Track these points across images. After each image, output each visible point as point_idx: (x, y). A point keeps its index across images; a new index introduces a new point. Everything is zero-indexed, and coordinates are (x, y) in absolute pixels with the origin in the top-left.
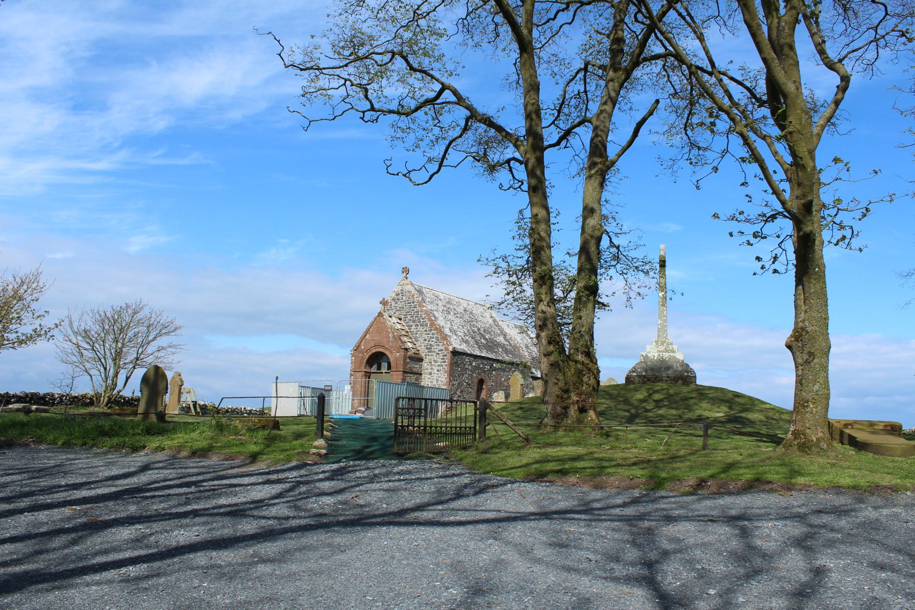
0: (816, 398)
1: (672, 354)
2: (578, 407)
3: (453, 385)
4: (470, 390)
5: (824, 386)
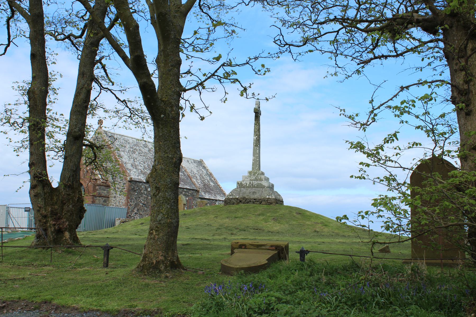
0: (159, 226)
1: (259, 182)
2: (55, 229)
3: (131, 205)
4: (146, 208)
5: (166, 216)
